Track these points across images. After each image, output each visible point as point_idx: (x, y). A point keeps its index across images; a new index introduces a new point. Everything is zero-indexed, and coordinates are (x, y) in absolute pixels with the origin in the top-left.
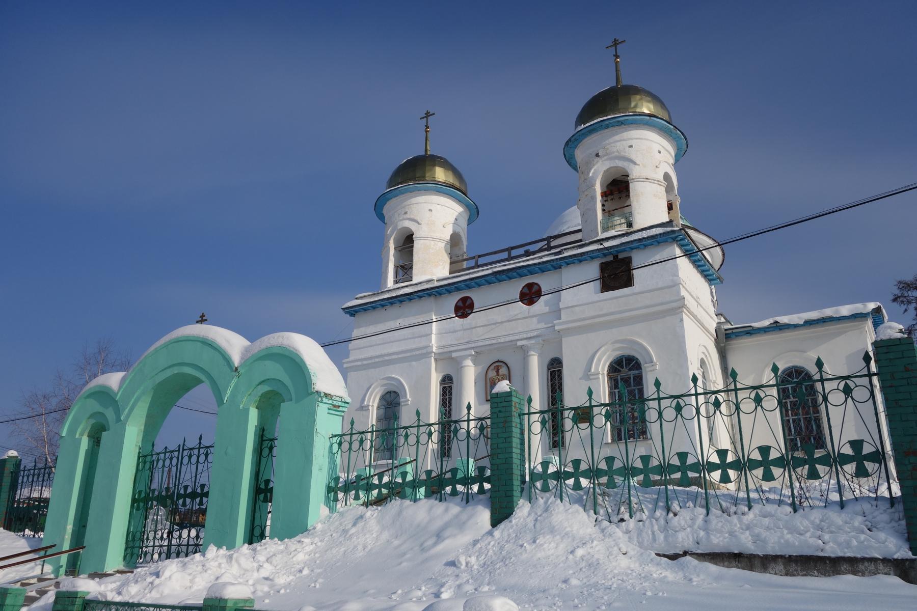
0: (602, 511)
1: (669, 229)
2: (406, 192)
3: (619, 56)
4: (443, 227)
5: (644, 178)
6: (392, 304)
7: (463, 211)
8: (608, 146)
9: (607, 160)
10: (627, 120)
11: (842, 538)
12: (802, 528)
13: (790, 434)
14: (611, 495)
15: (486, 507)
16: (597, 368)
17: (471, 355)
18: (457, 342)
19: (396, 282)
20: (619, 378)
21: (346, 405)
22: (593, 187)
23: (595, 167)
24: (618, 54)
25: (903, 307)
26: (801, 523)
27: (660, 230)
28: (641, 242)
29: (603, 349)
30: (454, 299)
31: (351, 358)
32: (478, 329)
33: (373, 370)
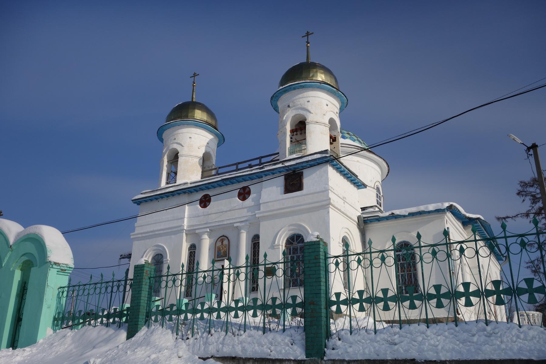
0: (180, 334)
1: (324, 155)
2: (176, 126)
3: (309, 43)
4: (198, 148)
5: (315, 122)
6: (162, 198)
7: (213, 138)
8: (295, 101)
9: (294, 109)
10: (306, 85)
11: (279, 349)
12: (264, 343)
13: (399, 284)
14: (188, 324)
15: (125, 331)
16: (279, 242)
17: (207, 232)
18: (199, 223)
19: (167, 183)
20: (292, 248)
21: (71, 269)
22: (285, 127)
23: (287, 114)
24: (309, 41)
25: (522, 198)
26: (264, 341)
27: (319, 156)
28: (308, 163)
29: (283, 230)
30: (199, 195)
31: (136, 232)
32: (212, 215)
33: (148, 240)
